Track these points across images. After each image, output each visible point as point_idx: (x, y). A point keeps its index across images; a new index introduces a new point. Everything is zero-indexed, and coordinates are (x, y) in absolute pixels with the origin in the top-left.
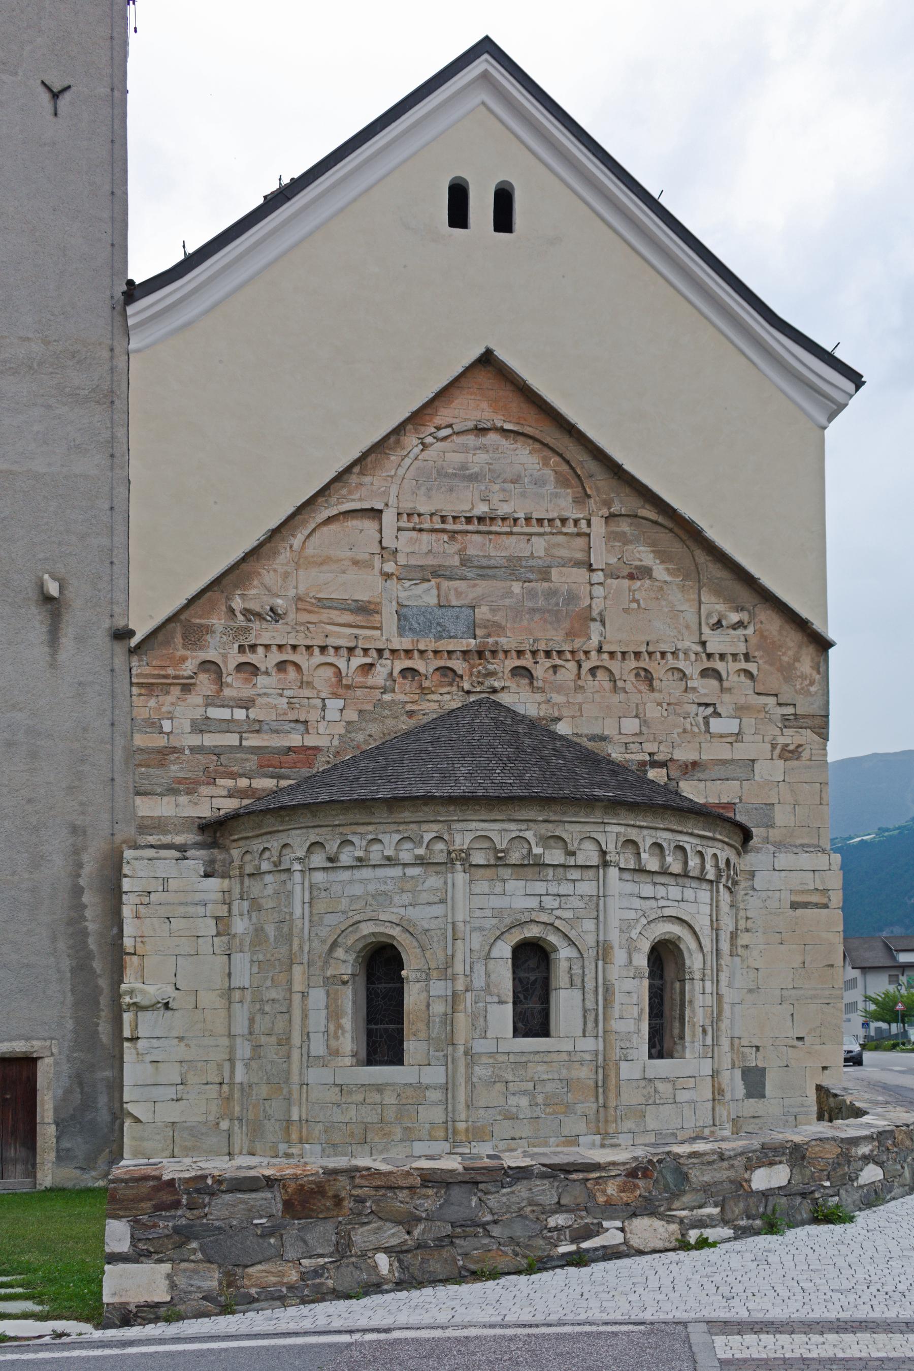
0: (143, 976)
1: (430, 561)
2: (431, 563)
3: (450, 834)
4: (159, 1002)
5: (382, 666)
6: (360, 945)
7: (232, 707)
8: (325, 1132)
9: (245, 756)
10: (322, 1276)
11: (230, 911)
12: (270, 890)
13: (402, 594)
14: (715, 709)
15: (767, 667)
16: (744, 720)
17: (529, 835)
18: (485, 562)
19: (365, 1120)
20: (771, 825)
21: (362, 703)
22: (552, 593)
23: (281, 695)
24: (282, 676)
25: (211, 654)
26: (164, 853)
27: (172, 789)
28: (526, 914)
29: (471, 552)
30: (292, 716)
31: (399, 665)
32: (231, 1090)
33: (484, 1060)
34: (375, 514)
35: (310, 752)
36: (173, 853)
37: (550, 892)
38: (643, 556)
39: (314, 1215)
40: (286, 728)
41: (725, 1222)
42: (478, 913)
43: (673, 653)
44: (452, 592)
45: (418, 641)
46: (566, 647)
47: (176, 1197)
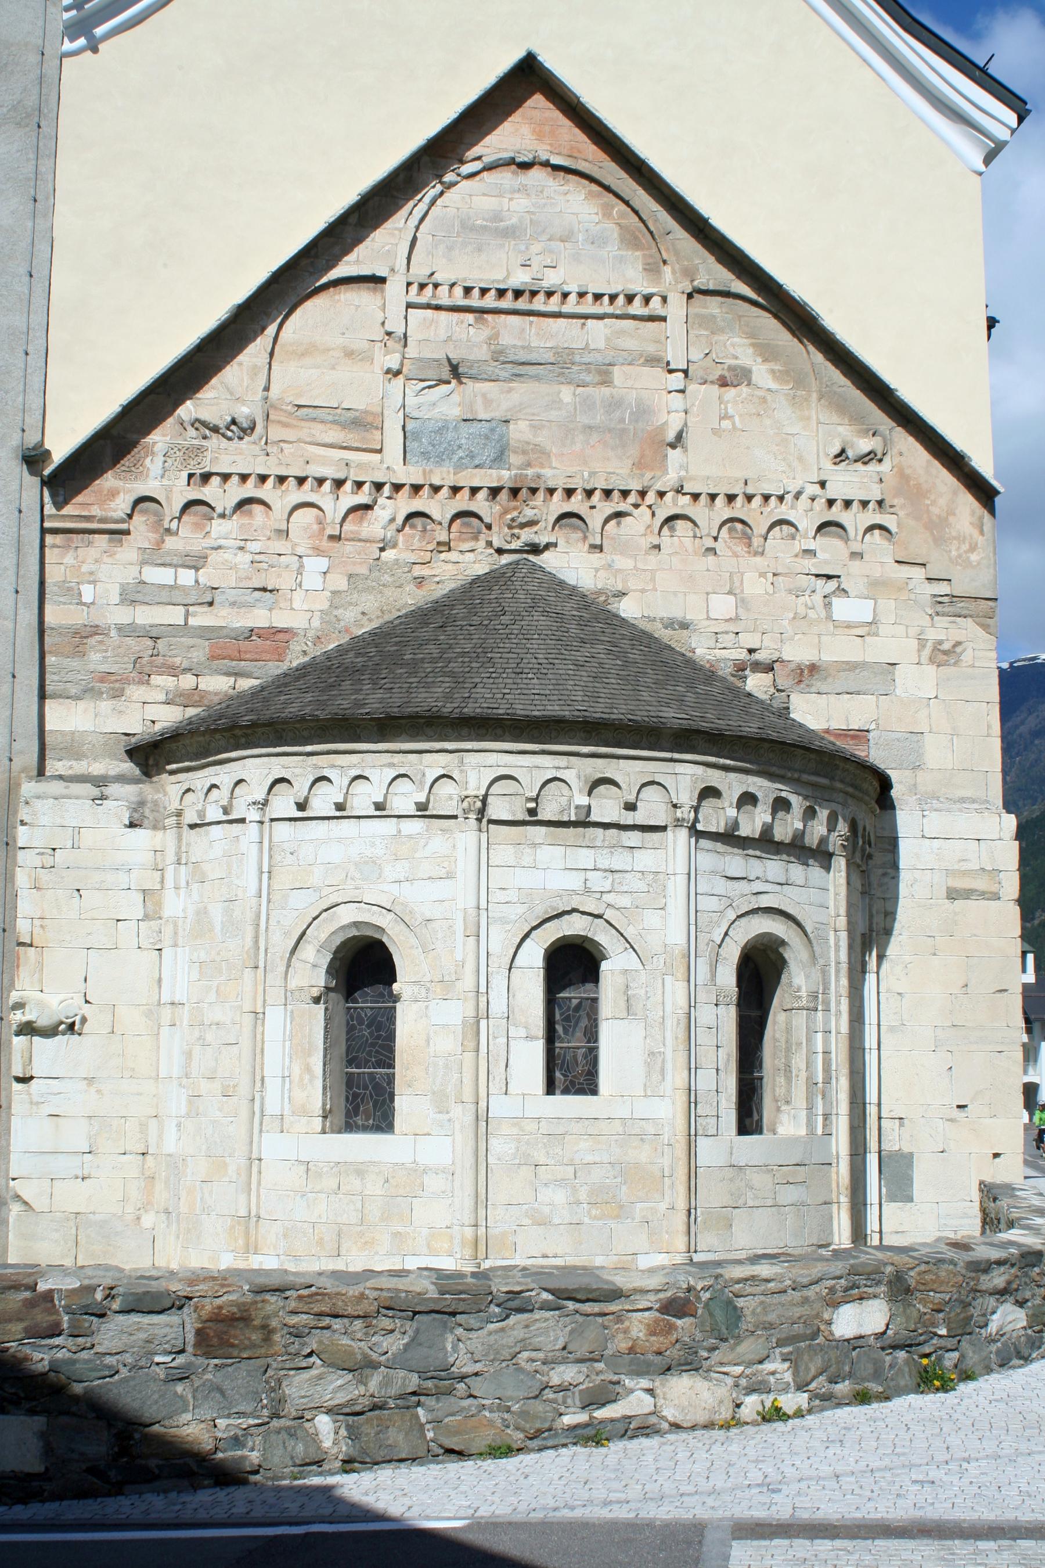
0: (41, 981)
3: (461, 771)
4: (62, 1023)
6: (338, 940)
7: (176, 566)
8: (285, 1236)
9: (191, 641)
10: (244, 1446)
11: (162, 882)
12: (217, 850)
15: (912, 523)
16: (879, 601)
17: (567, 775)
18: (523, 356)
19: (339, 1220)
21: (354, 563)
22: (614, 404)
23: (241, 548)
24: (245, 520)
27: (92, 689)
28: (565, 898)
29: (506, 340)
34: (377, 280)
35: (280, 636)
37: (599, 866)
38: (739, 351)
39: (235, 1353)
41: (801, 1387)
42: (501, 896)
44: (479, 400)
45: (431, 471)
47: (54, 1317)
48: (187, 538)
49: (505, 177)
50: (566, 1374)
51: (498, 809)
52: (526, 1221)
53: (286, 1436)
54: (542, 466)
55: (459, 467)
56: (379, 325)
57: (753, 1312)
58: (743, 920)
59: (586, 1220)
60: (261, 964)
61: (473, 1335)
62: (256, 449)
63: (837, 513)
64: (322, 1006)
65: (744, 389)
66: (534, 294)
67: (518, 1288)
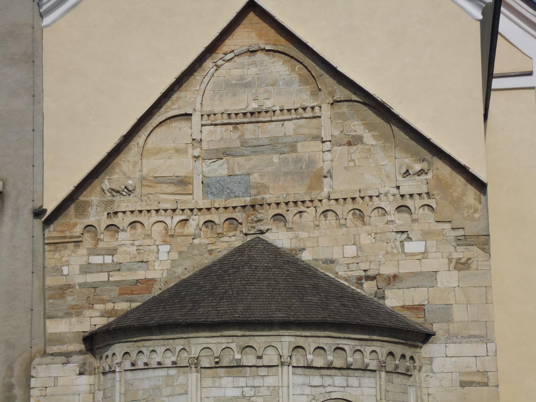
1: (222, 145)
2: (222, 146)
3: (189, 347)
5: (194, 220)
7: (104, 255)
13: (206, 169)
14: (408, 235)
16: (428, 242)
18: (256, 143)
20: (449, 321)
21: (181, 246)
22: (299, 160)
23: (133, 244)
24: (133, 231)
25: (92, 220)
29: (247, 136)
30: (138, 259)
31: (203, 219)
34: (187, 116)
35: (149, 282)
36: (63, 359)
37: (248, 385)
38: (357, 128)
40: (136, 267)
43: (378, 196)
44: (236, 165)
46: (307, 198)
48: (107, 241)
49: (245, 59)
51: (205, 363)
54: (265, 194)
55: (229, 197)
56: (190, 136)
62: (136, 199)
65: (360, 146)
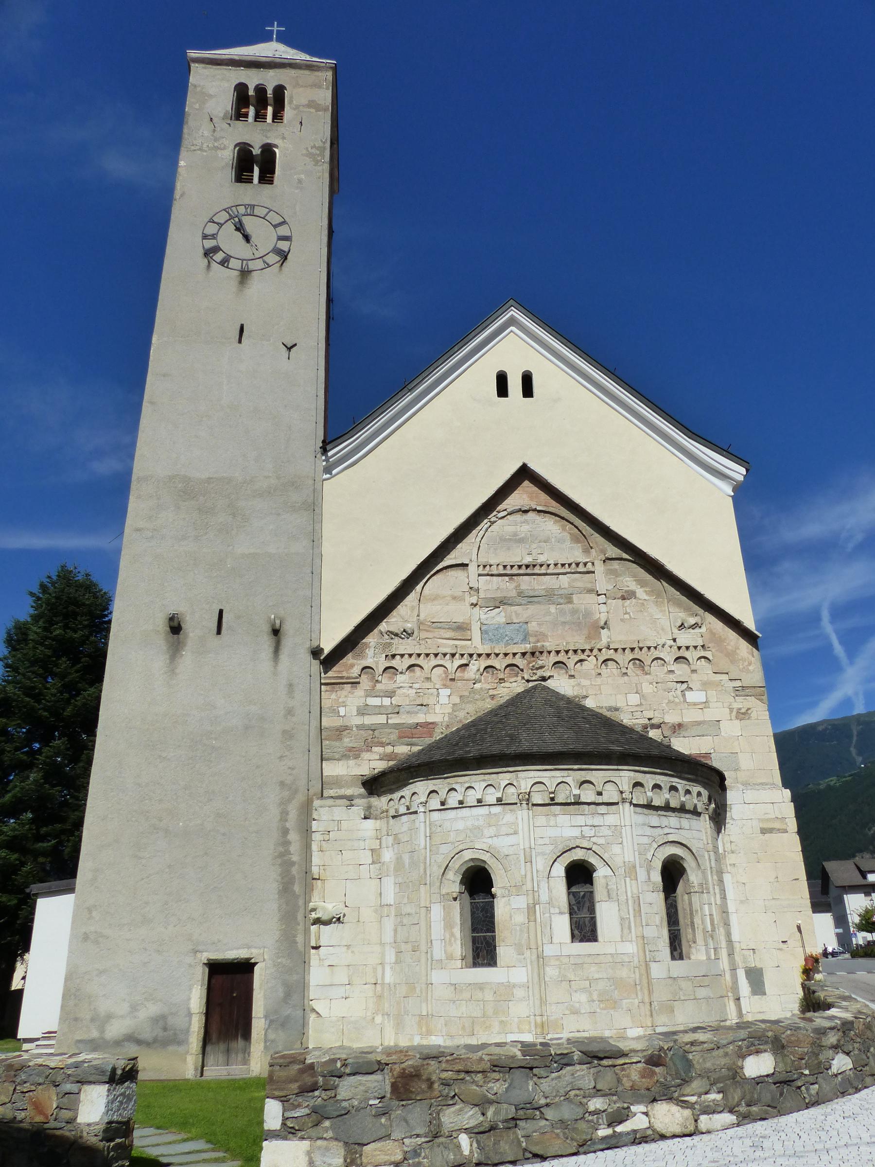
0: (324, 897)
1: (499, 595)
9: (390, 731)
11: (380, 845)
12: (405, 828)
13: (483, 617)
17: (569, 780)
19: (473, 1015)
22: (575, 612)
24: (412, 674)
25: (368, 662)
26: (339, 802)
29: (524, 587)
32: (383, 989)
33: (553, 962)
36: (345, 802)
38: (629, 584)
42: (541, 842)
48: (385, 683)
49: (518, 517)
50: (596, 1104)
51: (537, 799)
52: (567, 1012)
53: (443, 1149)
54: (544, 641)
55: (507, 644)
57: (698, 1062)
58: (661, 848)
59: (598, 1010)
60: (428, 882)
61: (542, 1081)
62: (415, 642)
63: (683, 653)
64: (458, 902)
66: (534, 566)
67: (565, 1052)
